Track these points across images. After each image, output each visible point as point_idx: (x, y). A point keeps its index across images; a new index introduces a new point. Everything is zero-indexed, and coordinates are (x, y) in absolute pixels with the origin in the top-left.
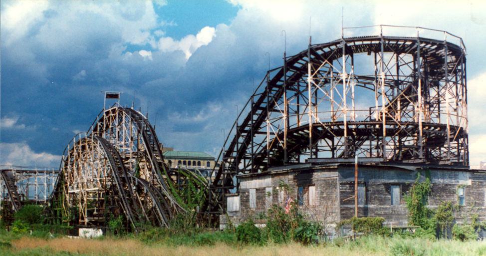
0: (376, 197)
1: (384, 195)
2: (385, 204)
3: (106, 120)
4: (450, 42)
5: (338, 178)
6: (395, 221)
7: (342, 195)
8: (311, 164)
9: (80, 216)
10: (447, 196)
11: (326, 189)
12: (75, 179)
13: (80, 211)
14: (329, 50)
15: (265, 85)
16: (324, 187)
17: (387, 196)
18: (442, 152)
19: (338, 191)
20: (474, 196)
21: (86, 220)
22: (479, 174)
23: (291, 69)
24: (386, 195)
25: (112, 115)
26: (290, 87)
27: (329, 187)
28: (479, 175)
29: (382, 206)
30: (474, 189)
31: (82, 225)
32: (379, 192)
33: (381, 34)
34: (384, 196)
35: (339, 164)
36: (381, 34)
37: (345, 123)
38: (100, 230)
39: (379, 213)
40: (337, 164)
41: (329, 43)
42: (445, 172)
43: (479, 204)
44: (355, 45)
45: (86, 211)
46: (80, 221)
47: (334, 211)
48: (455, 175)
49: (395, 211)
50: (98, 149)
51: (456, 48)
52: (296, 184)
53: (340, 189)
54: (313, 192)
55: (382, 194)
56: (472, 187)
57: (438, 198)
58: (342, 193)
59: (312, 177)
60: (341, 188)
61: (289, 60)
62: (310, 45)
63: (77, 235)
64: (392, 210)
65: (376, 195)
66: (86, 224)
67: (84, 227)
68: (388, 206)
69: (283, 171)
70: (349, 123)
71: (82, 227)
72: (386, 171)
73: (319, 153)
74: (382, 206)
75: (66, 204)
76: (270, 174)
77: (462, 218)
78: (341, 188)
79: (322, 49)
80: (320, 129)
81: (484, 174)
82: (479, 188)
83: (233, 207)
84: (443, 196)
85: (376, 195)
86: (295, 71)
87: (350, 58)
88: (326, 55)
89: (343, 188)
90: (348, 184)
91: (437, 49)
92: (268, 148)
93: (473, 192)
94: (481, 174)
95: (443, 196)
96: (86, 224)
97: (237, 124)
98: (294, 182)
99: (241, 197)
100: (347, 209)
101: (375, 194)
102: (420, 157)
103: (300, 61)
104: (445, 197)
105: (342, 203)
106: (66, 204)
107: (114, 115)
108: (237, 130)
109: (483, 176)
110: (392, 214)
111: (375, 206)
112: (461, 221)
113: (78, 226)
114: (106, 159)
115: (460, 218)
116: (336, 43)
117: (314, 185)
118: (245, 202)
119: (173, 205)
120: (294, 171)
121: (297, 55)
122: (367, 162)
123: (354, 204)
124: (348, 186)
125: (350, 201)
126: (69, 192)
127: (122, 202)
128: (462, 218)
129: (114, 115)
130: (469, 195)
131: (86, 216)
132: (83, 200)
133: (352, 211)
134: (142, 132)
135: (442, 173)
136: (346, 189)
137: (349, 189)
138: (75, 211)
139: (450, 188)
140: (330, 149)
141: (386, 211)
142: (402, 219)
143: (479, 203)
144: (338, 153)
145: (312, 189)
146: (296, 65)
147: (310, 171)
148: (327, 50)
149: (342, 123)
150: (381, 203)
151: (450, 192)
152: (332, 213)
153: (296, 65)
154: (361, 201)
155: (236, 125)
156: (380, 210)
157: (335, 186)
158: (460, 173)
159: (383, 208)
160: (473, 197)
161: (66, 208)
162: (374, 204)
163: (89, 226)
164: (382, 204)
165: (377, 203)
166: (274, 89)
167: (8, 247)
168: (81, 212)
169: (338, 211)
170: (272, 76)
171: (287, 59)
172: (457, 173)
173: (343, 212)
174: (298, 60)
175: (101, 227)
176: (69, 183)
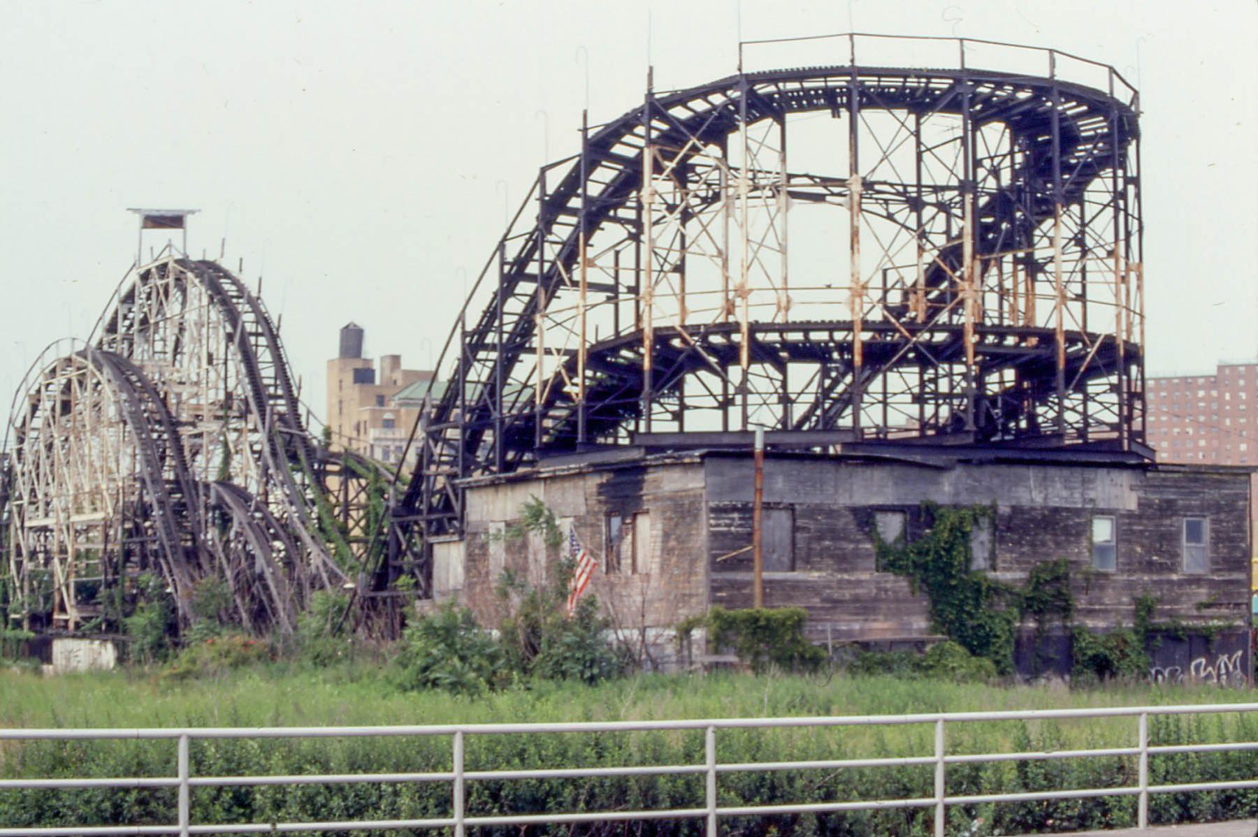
0: (828, 548)
1: (852, 541)
2: (854, 569)
3: (158, 293)
4: (1070, 81)
5: (704, 492)
6: (886, 620)
7: (716, 545)
8: (643, 450)
9: (57, 599)
10: (1058, 544)
11: (677, 525)
12: (43, 483)
13: (57, 586)
14: (707, 106)
15: (534, 208)
16: (671, 519)
17: (861, 546)
18: (1080, 408)
19: (704, 532)
20: (1145, 541)
21: (73, 615)
22: (1163, 475)
23: (604, 163)
24: (858, 542)
25: (159, 282)
26: (612, 213)
27: (683, 518)
28: (1164, 479)
29: (846, 577)
30: (1145, 522)
31: (63, 631)
32: (835, 535)
33: (852, 61)
34: (851, 546)
35: (704, 451)
36: (852, 61)
37: (745, 328)
38: (110, 646)
39: (836, 596)
40: (697, 453)
41: (704, 87)
42: (1052, 471)
43: (1162, 568)
44: (779, 92)
45: (72, 586)
46: (56, 616)
47: (693, 591)
48: (1084, 481)
49: (886, 591)
50: (107, 389)
51: (1096, 97)
52: (604, 508)
53: (711, 526)
54: (648, 529)
55: (844, 539)
56: (1140, 517)
57: (1025, 549)
58: (715, 536)
59: (641, 489)
60: (712, 522)
61: (597, 134)
62: (650, 94)
63: (48, 659)
64: (879, 589)
65: (827, 543)
66: (71, 625)
67: (67, 637)
68: (865, 576)
69: (569, 469)
70: (754, 328)
71: (59, 636)
72: (860, 469)
73: (687, 413)
74: (846, 577)
75: (19, 565)
76: (539, 479)
77: (1105, 611)
78: (712, 522)
79: (724, 93)
80: (676, 343)
81: (1176, 475)
82: (1161, 517)
83: (448, 580)
84: (1044, 544)
85: (827, 543)
86: (621, 167)
87: (777, 127)
88: (695, 123)
89: (721, 522)
90: (734, 509)
91: (1036, 98)
92: (537, 401)
93: (1141, 531)
94: (1170, 475)
95: (1044, 544)
96: (71, 625)
97: (463, 327)
98: (600, 502)
99: (469, 546)
100: (733, 585)
101: (820, 538)
102: (967, 428)
103: (627, 138)
104: (1051, 544)
105: (717, 566)
106: (19, 565)
107: (163, 282)
108: (463, 343)
109: (1176, 480)
110: (876, 599)
111: (824, 574)
112: (1103, 620)
113: (50, 631)
114: (125, 423)
115: (1100, 611)
116: (721, 87)
117: (647, 512)
118: (475, 559)
119: (317, 568)
120: (598, 469)
121: (617, 121)
122: (790, 445)
123: (751, 569)
124: (736, 515)
125: (741, 561)
126: (27, 524)
127: (165, 557)
128: (1105, 611)
129: (163, 282)
130: (1129, 541)
131: (70, 603)
132: (63, 551)
133: (746, 591)
134: (237, 339)
135: (1041, 475)
136: (726, 525)
137: (740, 526)
138: (43, 587)
139: (1068, 518)
140: (716, 404)
141: (859, 591)
142: (908, 614)
143: (1161, 564)
144: (798, 411)
145: (643, 523)
146: (617, 149)
147: (635, 471)
148: (699, 105)
149: (736, 328)
150: (844, 566)
151: (1066, 531)
152: (691, 596)
153: (617, 149)
154: (779, 560)
155: (459, 330)
156: (841, 588)
157: (696, 517)
158: (1102, 473)
159: (849, 582)
160: (1142, 546)
161: (18, 573)
162: (820, 570)
163: (80, 632)
164: (845, 571)
165: (828, 566)
166: (562, 218)
167: (472, 695)
168: (59, 589)
169: (703, 591)
170: (555, 180)
171: (591, 134)
172: (1089, 473)
173: (719, 594)
174: (623, 135)
175: (111, 636)
176: (26, 498)
